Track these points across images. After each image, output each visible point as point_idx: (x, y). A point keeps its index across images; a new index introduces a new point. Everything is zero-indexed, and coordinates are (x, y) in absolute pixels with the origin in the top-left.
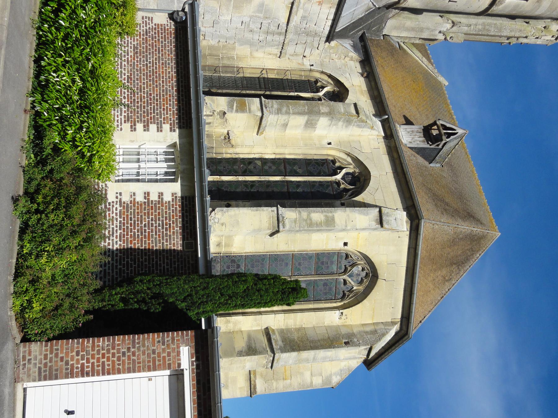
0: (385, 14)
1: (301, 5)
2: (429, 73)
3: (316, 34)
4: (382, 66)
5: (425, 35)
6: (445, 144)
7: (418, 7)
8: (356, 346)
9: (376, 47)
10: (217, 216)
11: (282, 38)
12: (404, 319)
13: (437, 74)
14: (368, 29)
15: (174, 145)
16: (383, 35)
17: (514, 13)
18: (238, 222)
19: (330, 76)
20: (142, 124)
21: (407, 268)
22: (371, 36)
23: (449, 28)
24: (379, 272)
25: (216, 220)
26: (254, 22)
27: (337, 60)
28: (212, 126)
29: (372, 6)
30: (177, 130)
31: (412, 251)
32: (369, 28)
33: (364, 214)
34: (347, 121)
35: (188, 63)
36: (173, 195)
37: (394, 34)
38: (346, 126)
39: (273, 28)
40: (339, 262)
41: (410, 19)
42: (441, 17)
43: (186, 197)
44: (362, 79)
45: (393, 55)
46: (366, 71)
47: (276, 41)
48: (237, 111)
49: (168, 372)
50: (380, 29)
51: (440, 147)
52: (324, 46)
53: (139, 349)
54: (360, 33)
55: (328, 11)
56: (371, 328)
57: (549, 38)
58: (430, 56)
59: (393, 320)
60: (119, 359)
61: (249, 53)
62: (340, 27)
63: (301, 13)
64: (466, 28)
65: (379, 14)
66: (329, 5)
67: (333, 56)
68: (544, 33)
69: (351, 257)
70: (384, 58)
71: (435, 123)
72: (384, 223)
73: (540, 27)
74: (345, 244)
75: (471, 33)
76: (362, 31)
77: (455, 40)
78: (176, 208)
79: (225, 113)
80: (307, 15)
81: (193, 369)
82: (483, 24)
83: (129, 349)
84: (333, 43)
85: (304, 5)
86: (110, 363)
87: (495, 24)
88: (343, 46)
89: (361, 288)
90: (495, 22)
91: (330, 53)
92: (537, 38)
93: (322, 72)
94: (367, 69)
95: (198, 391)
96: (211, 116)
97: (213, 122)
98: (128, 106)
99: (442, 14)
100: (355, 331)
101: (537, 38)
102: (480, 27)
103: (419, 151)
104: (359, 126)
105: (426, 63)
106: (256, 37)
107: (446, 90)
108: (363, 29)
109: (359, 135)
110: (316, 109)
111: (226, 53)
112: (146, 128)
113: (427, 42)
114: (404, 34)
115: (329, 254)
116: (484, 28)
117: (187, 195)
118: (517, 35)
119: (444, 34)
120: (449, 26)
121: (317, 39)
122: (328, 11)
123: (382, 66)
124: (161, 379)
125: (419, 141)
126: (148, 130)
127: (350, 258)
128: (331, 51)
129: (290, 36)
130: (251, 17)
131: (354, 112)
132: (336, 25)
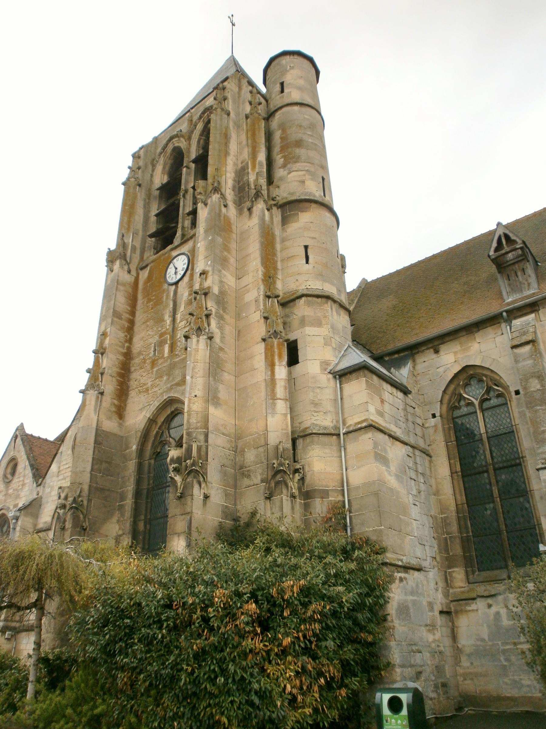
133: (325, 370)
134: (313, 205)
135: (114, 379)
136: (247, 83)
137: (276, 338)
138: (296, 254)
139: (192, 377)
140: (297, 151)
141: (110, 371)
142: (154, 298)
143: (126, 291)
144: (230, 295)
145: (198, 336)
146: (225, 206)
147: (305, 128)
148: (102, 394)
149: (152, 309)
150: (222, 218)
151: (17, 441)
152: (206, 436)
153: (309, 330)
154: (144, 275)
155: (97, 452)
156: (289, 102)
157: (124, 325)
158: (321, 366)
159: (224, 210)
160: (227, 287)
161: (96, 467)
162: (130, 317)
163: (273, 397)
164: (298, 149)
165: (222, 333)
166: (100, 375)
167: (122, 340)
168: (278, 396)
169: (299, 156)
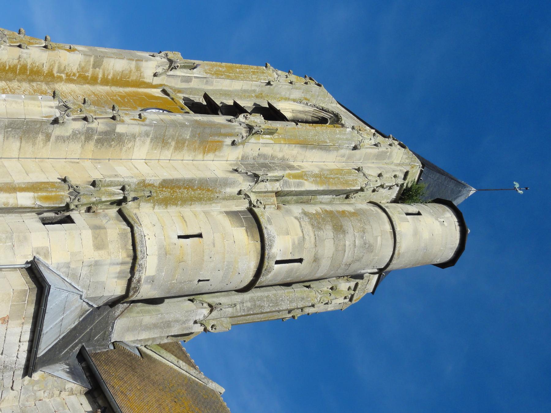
0: (108, 313)
2: (194, 381)
3: (5, 367)
4: (122, 392)
5: (176, 330)
7: (157, 297)
9: (107, 364)
13: (206, 380)
14: (89, 340)
16: (113, 343)
17: (288, 280)
22: (95, 349)
23: (206, 315)
27: (47, 400)
29: (87, 307)
32: (89, 338)
37: (129, 338)
41: (149, 312)
42: (192, 301)
45: (134, 370)
46: (99, 407)
50: (106, 336)
52: (21, 382)
54: (77, 349)
55: (18, 330)
57: (341, 300)
58: (188, 354)
62: (43, 350)
64: (230, 310)
65: (99, 316)
66: (20, 321)
67: (41, 394)
68: (333, 296)
70: (123, 379)
73: (325, 289)
75: (239, 314)
76: (80, 346)
77: (219, 329)
82: (252, 300)
84: (36, 376)
87: (267, 297)
88: (53, 376)
90: (266, 294)
91: (35, 392)
92: (327, 303)
94: (100, 402)
99: (191, 298)
101: (327, 303)
102: (249, 304)
105: (185, 368)
107: (225, 400)
108: (80, 342)
113: (180, 340)
114: (144, 336)
116: (255, 305)
118: (300, 305)
119: (202, 324)
120: (206, 311)
122: (18, 330)
123: (122, 392)
128: (35, 388)
132: (37, 348)
133: (38, 253)
134: (258, 245)
135: (16, 61)
136: (405, 171)
137: (70, 194)
138: (188, 224)
139: (5, 100)
140: (329, 227)
141: (25, 56)
142: (126, 100)
143: (130, 72)
144: (121, 149)
145: (58, 107)
146: (233, 143)
147: (362, 237)
149: (113, 99)
150: (216, 138)
151: (137, 351)
153: (88, 235)
154: (157, 92)
156: (393, 220)
157: (87, 71)
158: (43, 248)
159: (229, 141)
160: (130, 145)
162: (100, 79)
164: (330, 228)
165: (68, 138)
166: (18, 44)
167: (68, 70)
169: (322, 229)
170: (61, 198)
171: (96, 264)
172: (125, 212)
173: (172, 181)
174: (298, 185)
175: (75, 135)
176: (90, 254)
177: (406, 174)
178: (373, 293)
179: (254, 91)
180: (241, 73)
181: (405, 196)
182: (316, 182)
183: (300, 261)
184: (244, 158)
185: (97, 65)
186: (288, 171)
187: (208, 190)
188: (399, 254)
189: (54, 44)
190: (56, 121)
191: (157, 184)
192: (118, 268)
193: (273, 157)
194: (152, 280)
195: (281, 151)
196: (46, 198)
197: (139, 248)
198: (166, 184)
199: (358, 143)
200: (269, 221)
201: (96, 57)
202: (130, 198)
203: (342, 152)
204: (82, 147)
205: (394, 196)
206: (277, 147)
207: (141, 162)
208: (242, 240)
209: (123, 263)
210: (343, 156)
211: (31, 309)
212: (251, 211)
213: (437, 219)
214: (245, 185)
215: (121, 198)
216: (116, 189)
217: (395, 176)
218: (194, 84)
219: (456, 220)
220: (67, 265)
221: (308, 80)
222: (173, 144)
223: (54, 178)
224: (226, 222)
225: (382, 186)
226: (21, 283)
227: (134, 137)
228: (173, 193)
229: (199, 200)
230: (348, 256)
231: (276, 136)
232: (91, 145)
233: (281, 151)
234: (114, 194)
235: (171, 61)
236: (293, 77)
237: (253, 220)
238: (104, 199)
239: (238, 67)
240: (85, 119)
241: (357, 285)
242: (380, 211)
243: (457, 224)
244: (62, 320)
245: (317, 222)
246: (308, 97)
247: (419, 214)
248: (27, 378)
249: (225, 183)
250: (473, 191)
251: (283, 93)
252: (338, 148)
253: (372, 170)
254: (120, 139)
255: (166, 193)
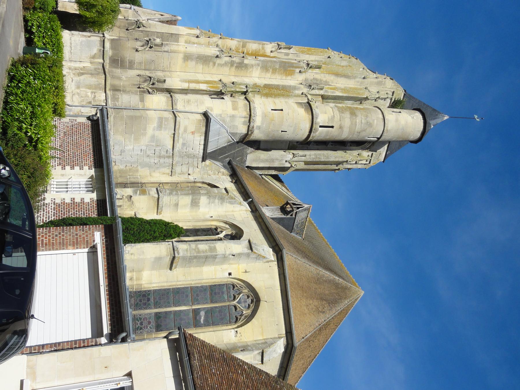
0: (243, 149)
1: (180, 135)
3: (194, 156)
6: (296, 213)
8: (250, 350)
10: (127, 249)
11: (171, 160)
12: (288, 334)
15: (92, 177)
18: (143, 252)
19: (226, 223)
20: (69, 167)
21: (281, 290)
24: (261, 295)
25: (127, 252)
26: (149, 150)
28: (122, 209)
29: (231, 140)
30: (94, 169)
31: (282, 276)
33: (238, 244)
34: (221, 199)
35: (100, 135)
36: (91, 199)
38: (221, 203)
39: (163, 153)
40: (228, 292)
43: (100, 200)
44: (232, 184)
47: (167, 163)
48: (140, 195)
49: (86, 250)
51: (294, 216)
53: (66, 233)
55: (199, 138)
56: (264, 341)
59: (280, 336)
60: (53, 238)
61: (149, 174)
63: (181, 141)
65: (238, 148)
69: (237, 286)
71: (287, 203)
72: (253, 249)
74: (230, 274)
78: (93, 206)
79: (131, 196)
80: (185, 142)
81: (103, 243)
82: (315, 154)
83: (60, 233)
84: (208, 162)
85: (182, 135)
86: (47, 240)
88: (215, 164)
89: (249, 312)
93: (203, 183)
95: (107, 253)
96: (121, 199)
97: (123, 205)
98: (60, 158)
100: (249, 344)
102: (313, 157)
103: (279, 220)
104: (231, 203)
106: (152, 161)
109: (233, 211)
110: (197, 192)
111: (132, 175)
112: (72, 168)
115: (219, 285)
117: (101, 198)
119: (289, 163)
120: (291, 156)
121: (196, 160)
124: (81, 256)
125: (279, 215)
126: (74, 169)
127: (236, 288)
129: (176, 159)
130: (147, 146)
131: (225, 192)
134: (311, 116)
145: (218, 51)
146: (300, 72)
148: (197, 37)
152: (167, 52)
155: (167, 35)
157: (239, 49)
159: (298, 70)
160: (251, 70)
161: (159, 35)
163: (190, 82)
165: (223, 65)
168: (190, 84)
170: (218, 88)
171: (233, 117)
172: (248, 98)
173: (269, 85)
174: (333, 93)
175: (226, 64)
176: (230, 111)
177: (393, 93)
178: (383, 162)
179: (322, 61)
180: (314, 52)
181: (395, 104)
182: (342, 92)
183: (332, 127)
184: (306, 80)
185: (244, 46)
186: (328, 86)
187: (287, 91)
188: (387, 130)
189: (224, 37)
190: (217, 57)
191: (262, 86)
192: (243, 120)
193: (321, 80)
194: (259, 128)
195: (325, 77)
196: (212, 87)
197: (252, 112)
198: (266, 86)
199: (366, 76)
200: (317, 107)
201: (243, 42)
202: (249, 91)
203: (357, 79)
204: (230, 69)
205: (388, 105)
206: (322, 75)
207: (256, 77)
208: (303, 115)
209: (245, 117)
210: (358, 82)
211: (204, 129)
212: (308, 103)
213: (410, 115)
214: (305, 90)
215: (245, 90)
216: (244, 87)
217: (387, 93)
218: (290, 57)
219: (421, 117)
220: (220, 115)
221: (351, 56)
222: (271, 70)
223: (217, 79)
224: (295, 106)
225: (379, 98)
226: (200, 117)
227: (252, 66)
228: (269, 91)
229: (283, 96)
230: (358, 128)
231: (322, 70)
232: (233, 69)
233: (325, 77)
234: (242, 88)
235: (279, 45)
236: (342, 55)
237: (309, 106)
238: (237, 90)
239: (313, 49)
240: (230, 56)
241: (372, 154)
242: (377, 109)
243: (422, 119)
244: (218, 139)
245: (342, 110)
246: (350, 65)
247: (400, 112)
248: (204, 163)
249: (295, 88)
250: (446, 118)
251: (337, 63)
252: (355, 78)
253: (374, 89)
254: (246, 66)
255: (266, 91)
